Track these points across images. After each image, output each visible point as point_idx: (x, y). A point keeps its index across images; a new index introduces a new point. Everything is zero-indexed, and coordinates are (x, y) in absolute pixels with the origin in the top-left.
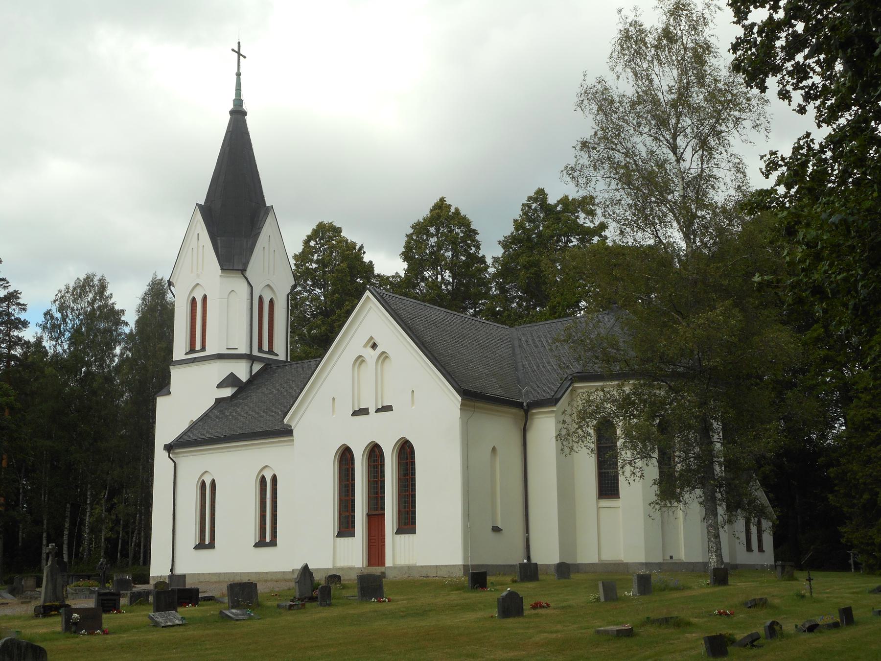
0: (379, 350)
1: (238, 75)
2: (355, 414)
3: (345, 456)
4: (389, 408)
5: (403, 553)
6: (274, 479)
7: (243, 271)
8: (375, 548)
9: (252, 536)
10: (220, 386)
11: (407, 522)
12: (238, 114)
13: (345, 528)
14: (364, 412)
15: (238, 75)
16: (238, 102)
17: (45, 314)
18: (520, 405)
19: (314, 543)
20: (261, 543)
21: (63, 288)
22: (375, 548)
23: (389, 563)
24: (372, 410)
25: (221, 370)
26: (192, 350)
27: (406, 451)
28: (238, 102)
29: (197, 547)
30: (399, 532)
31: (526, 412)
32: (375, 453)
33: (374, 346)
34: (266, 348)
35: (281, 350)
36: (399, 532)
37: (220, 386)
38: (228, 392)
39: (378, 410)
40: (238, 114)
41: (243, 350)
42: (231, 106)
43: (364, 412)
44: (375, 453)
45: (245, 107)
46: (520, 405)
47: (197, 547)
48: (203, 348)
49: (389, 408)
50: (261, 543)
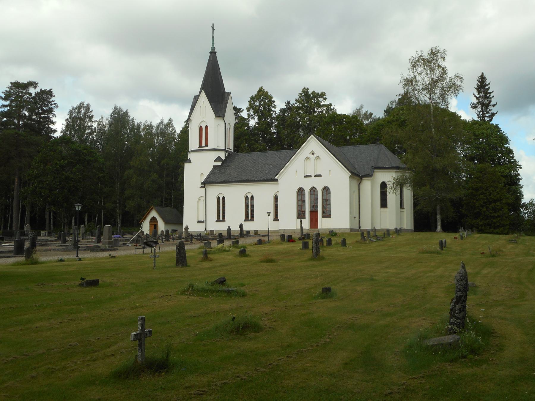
0: (315, 156)
1: (213, 37)
2: (305, 177)
3: (301, 191)
4: (320, 176)
5: (324, 224)
6: (224, 198)
7: (223, 117)
8: (314, 222)
9: (215, 218)
10: (215, 161)
11: (327, 214)
12: (213, 53)
13: (301, 215)
14: (310, 176)
15: (213, 37)
16: (213, 48)
17: (66, 120)
18: (359, 176)
19: (290, 222)
20: (218, 220)
21: (71, 109)
22: (314, 222)
23: (319, 227)
24: (313, 176)
25: (216, 155)
26: (201, 146)
27: (326, 190)
28: (213, 48)
29: (217, 221)
30: (323, 217)
31: (361, 179)
32: (313, 190)
33: (313, 154)
34: (204, 145)
35: (232, 147)
36: (323, 217)
37: (215, 161)
38: (219, 163)
39: (315, 176)
40: (213, 53)
41: (223, 148)
42: (210, 51)
43: (310, 176)
44: (313, 190)
45: (216, 50)
46: (359, 176)
47: (217, 221)
48: (206, 145)
49: (320, 176)
50: (218, 220)
